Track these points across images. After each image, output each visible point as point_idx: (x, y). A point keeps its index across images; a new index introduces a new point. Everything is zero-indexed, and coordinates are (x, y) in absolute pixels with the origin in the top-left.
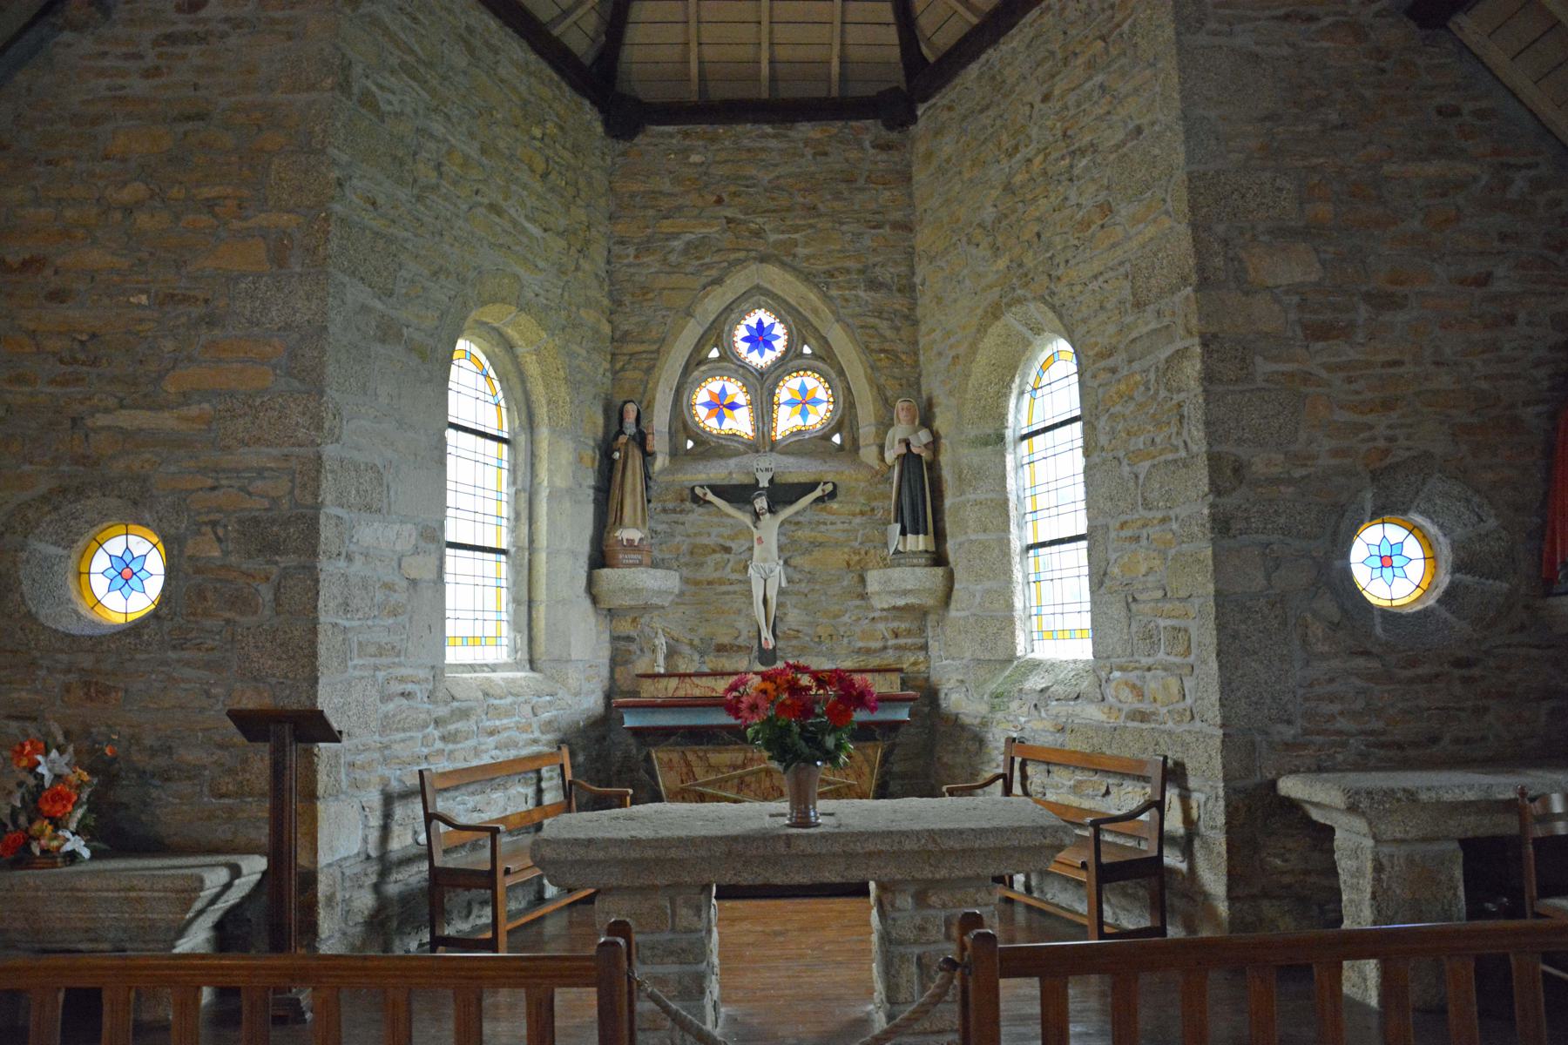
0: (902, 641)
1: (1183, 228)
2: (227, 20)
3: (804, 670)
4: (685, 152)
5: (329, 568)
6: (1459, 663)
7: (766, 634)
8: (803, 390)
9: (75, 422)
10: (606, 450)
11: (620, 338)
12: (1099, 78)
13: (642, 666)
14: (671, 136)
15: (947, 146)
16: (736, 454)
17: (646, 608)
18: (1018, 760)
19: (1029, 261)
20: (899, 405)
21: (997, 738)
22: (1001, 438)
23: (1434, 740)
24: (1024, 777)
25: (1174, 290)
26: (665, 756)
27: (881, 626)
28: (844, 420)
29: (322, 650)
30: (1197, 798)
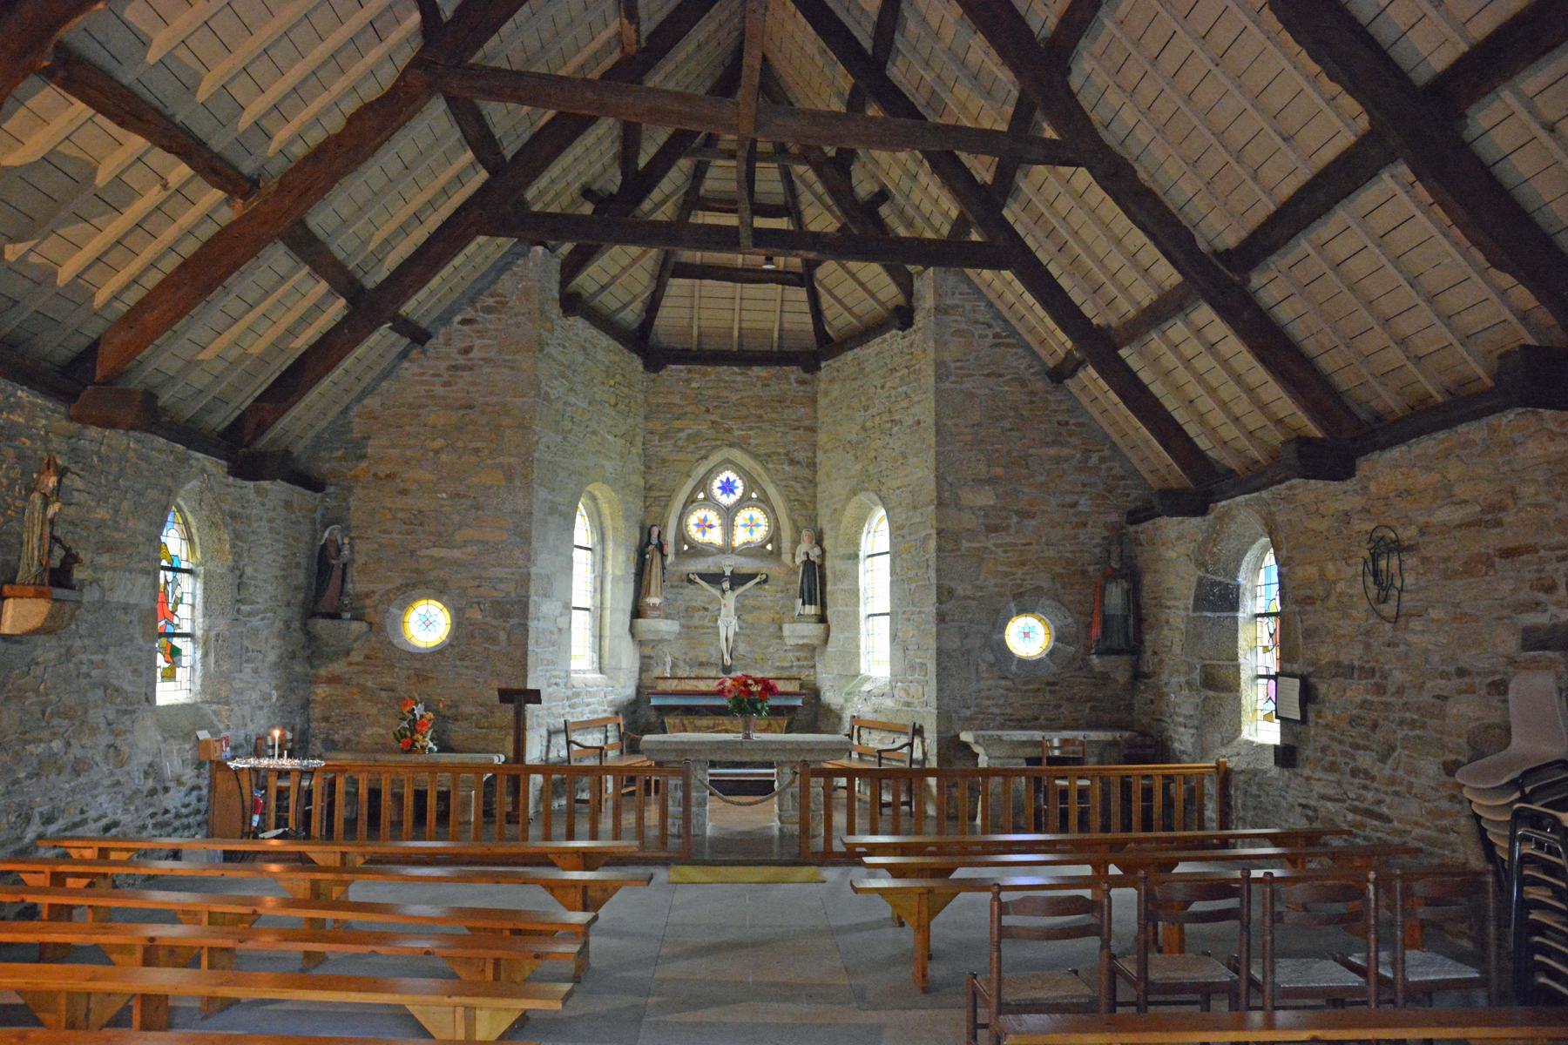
0: (801, 663)
1: (932, 476)
2: (482, 359)
3: (750, 677)
4: (688, 381)
5: (532, 624)
6: (1049, 684)
7: (726, 657)
8: (751, 519)
9: (412, 553)
10: (641, 553)
11: (649, 488)
12: (905, 388)
13: (657, 672)
14: (681, 371)
15: (836, 391)
16: (712, 554)
17: (661, 641)
18: (856, 727)
19: (871, 468)
20: (804, 533)
21: (847, 716)
22: (857, 556)
23: (1036, 719)
24: (859, 736)
25: (928, 505)
26: (671, 721)
27: (790, 654)
28: (774, 537)
29: (529, 662)
30: (928, 741)
